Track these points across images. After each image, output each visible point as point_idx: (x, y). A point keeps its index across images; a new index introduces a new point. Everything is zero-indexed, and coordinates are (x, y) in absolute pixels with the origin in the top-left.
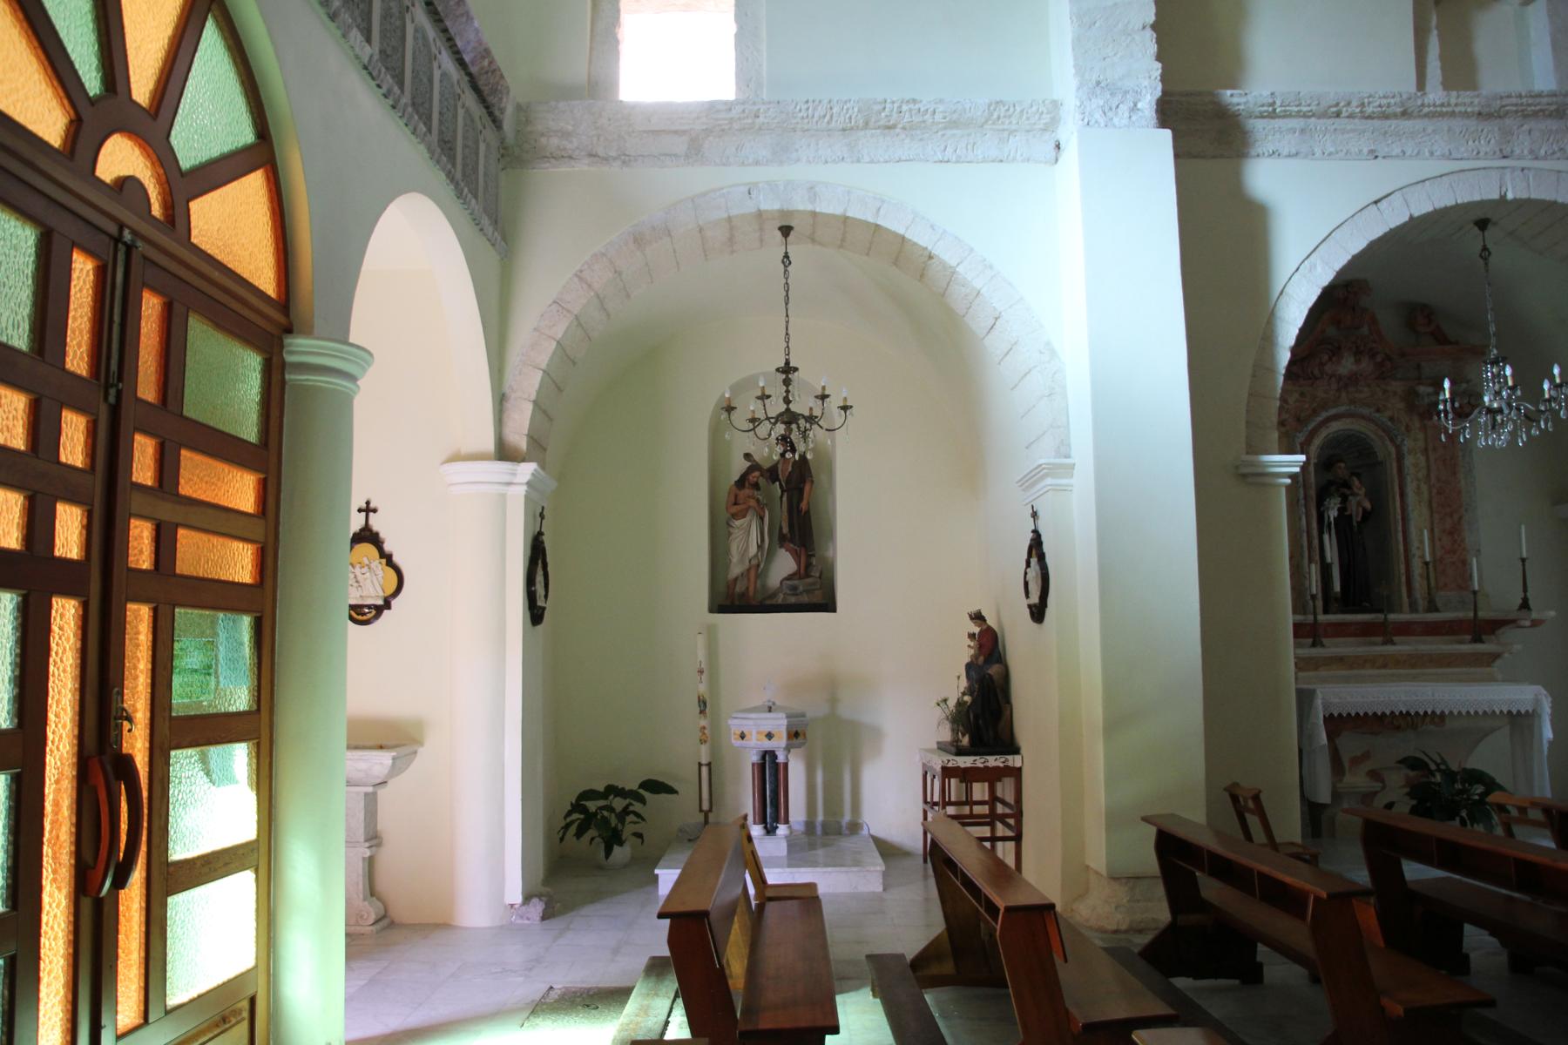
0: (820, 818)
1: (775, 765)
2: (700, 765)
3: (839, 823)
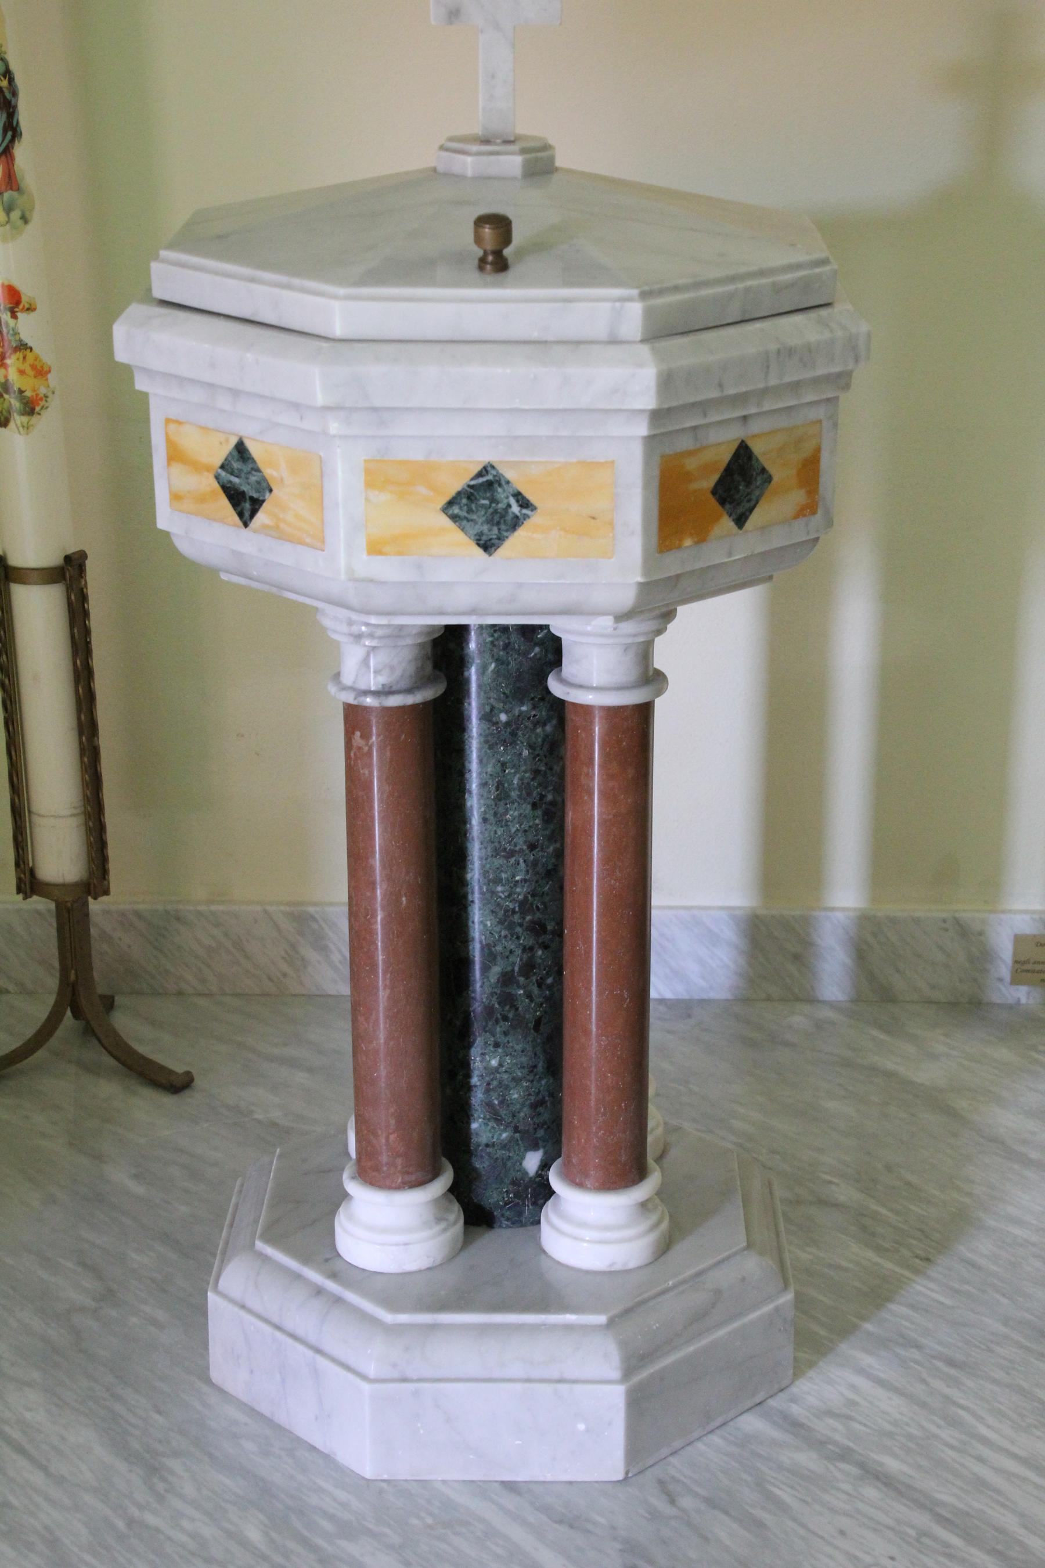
0: (845, 892)
1: (548, 728)
3: (971, 939)
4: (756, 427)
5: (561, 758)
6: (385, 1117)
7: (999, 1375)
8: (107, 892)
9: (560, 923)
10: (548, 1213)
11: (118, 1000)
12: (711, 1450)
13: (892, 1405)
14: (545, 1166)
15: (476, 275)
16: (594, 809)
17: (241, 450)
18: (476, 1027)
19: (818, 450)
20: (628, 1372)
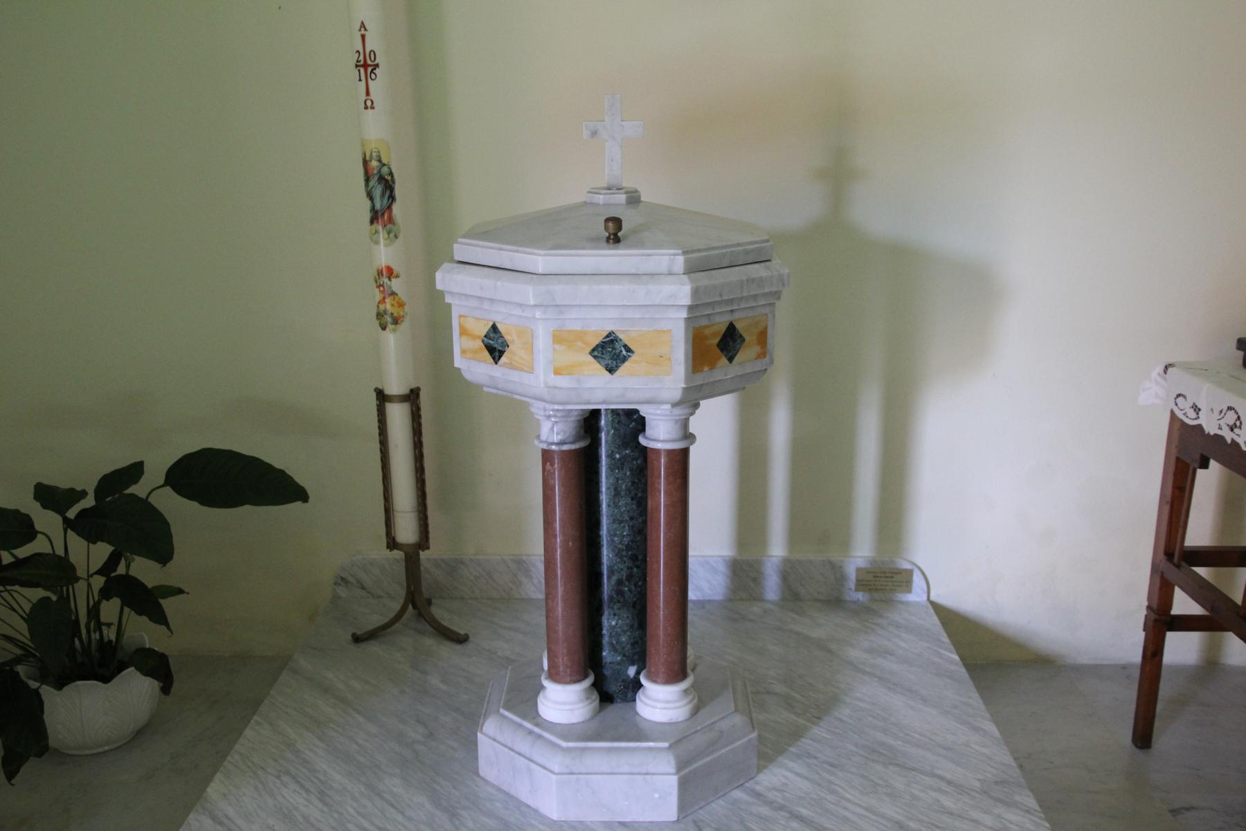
0: (777, 549)
1: (638, 460)
2: (382, 398)
3: (836, 570)
4: (737, 316)
5: (645, 476)
6: (562, 650)
7: (854, 770)
8: (428, 548)
9: (645, 556)
10: (640, 695)
11: (434, 601)
12: (718, 807)
13: (805, 785)
14: (638, 673)
15: (605, 244)
16: (661, 499)
17: (494, 328)
18: (605, 607)
19: (766, 328)
20: (679, 769)
